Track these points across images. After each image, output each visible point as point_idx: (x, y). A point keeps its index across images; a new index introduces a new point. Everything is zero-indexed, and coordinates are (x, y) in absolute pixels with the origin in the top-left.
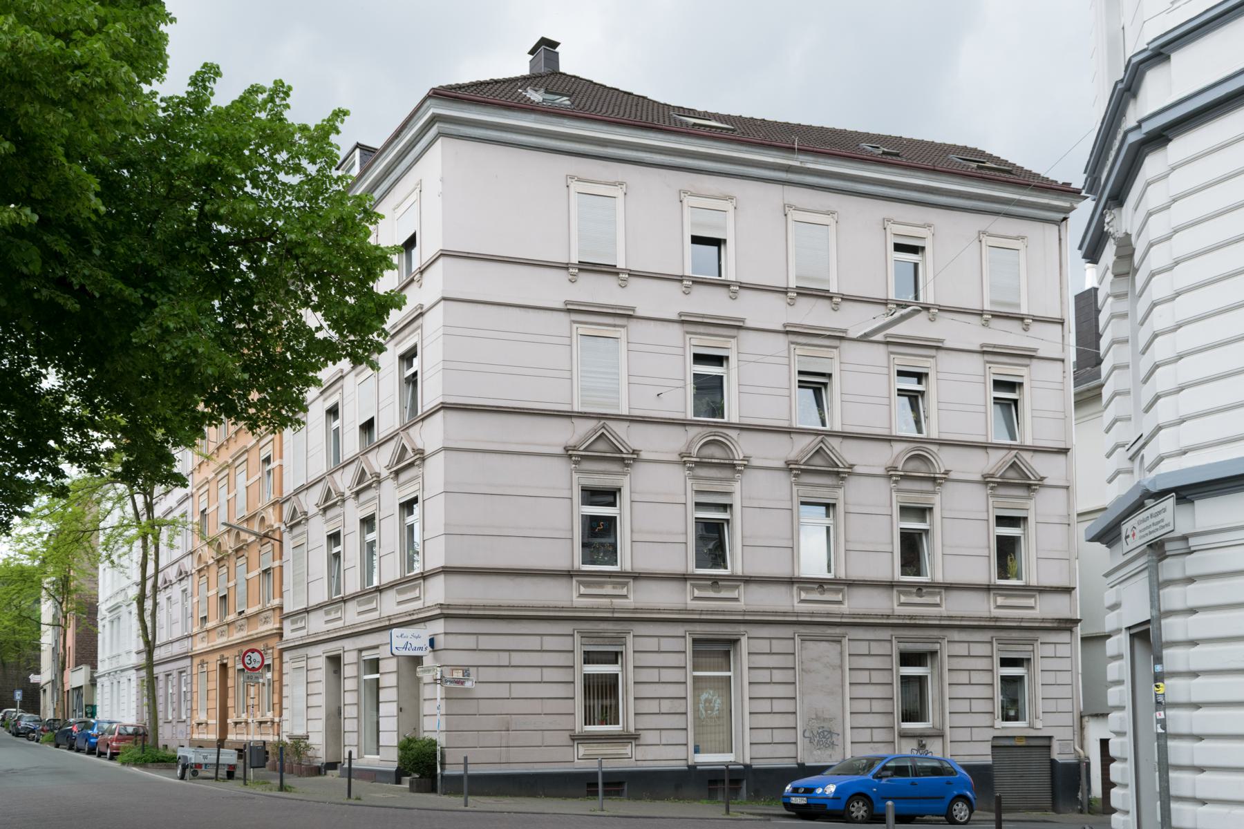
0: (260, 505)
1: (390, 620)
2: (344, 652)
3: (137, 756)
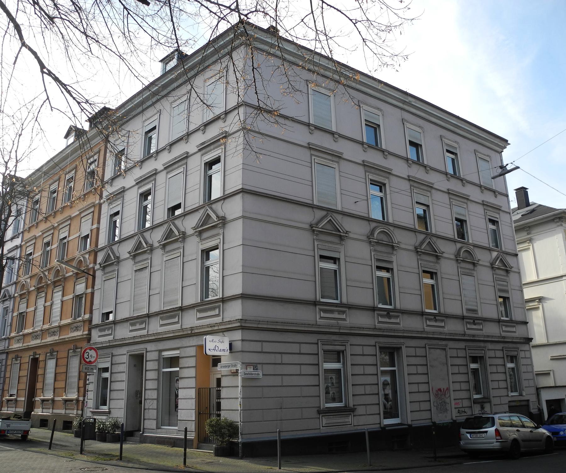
1: (340, 329)
2: (147, 352)
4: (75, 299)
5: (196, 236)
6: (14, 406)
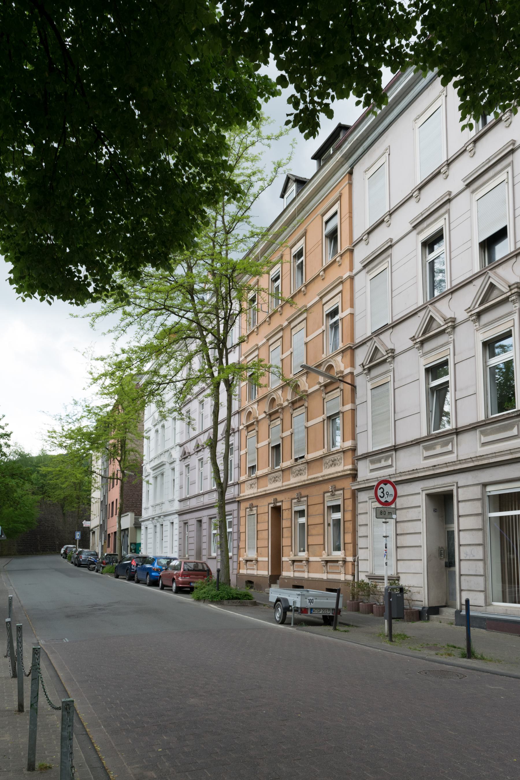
0: (324, 356)
2: (458, 487)
3: (214, 592)
4: (326, 422)
5: (472, 321)
6: (306, 569)
